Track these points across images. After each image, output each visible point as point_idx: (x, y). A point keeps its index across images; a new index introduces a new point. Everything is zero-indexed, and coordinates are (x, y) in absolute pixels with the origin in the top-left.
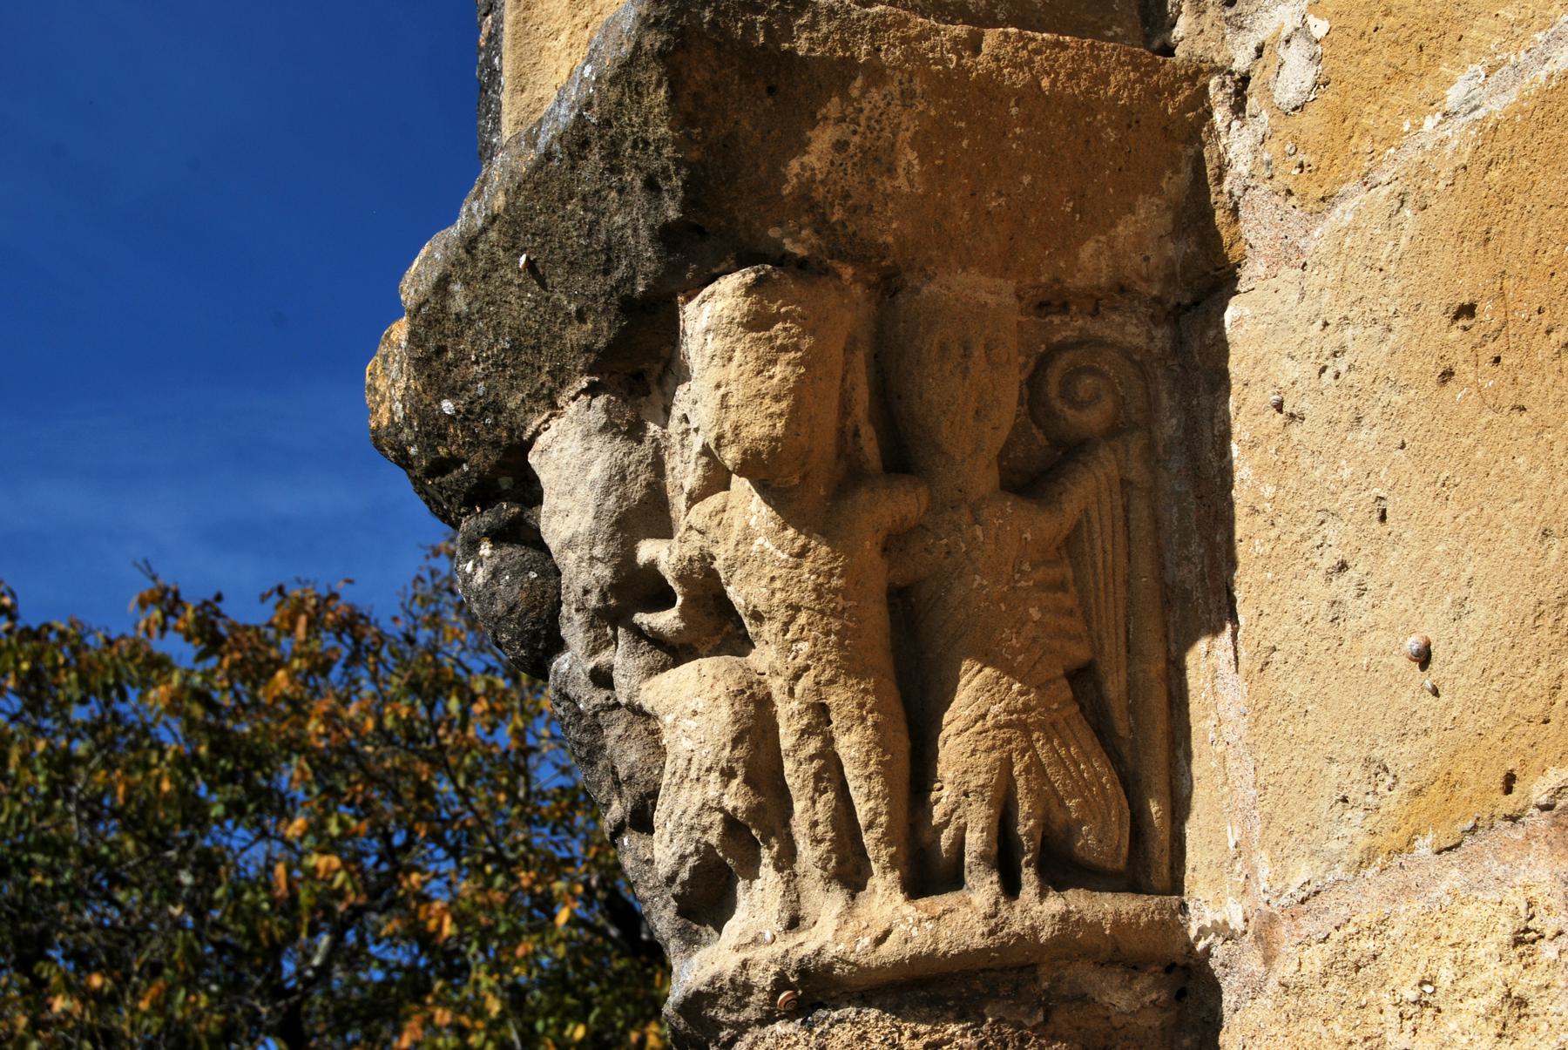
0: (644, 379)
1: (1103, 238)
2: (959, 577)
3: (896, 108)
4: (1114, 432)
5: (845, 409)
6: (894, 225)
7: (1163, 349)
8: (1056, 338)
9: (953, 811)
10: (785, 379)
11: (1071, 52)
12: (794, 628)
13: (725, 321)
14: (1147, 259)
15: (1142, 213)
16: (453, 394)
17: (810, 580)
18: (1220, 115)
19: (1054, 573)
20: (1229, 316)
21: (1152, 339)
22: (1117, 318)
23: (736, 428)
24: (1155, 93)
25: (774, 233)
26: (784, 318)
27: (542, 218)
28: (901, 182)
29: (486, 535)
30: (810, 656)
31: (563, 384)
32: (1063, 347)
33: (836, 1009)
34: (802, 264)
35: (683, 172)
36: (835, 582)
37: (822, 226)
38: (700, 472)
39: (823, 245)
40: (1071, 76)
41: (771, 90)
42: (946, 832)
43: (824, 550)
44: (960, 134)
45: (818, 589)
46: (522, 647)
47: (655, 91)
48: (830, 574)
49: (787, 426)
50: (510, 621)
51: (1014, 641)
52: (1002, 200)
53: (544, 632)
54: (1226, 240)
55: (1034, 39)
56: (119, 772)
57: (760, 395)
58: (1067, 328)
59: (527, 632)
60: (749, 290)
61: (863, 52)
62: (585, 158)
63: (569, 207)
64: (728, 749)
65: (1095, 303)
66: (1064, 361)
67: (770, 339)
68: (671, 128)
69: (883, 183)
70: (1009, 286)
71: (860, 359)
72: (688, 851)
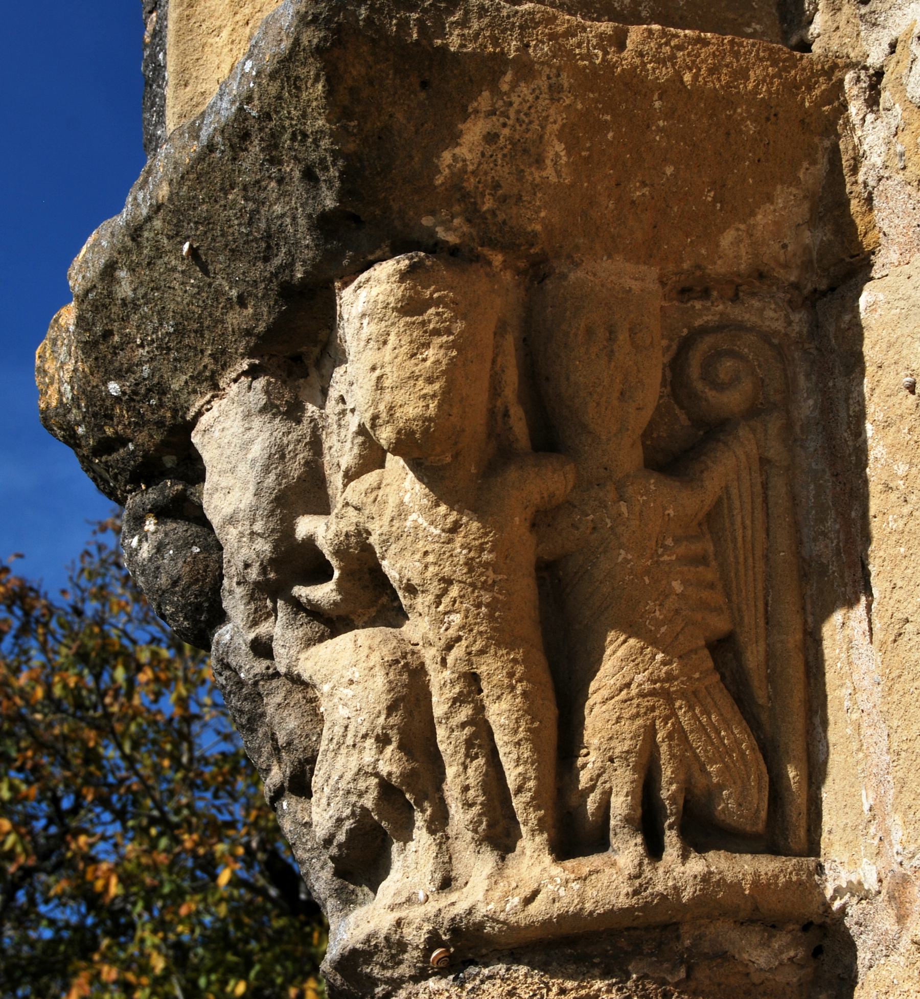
0: (302, 362)
1: (742, 227)
2: (605, 552)
5: (495, 390)
6: (543, 214)
7: (800, 333)
8: (698, 323)
9: (599, 776)
10: (437, 362)
11: (712, 48)
12: (446, 600)
13: (380, 306)
15: (780, 203)
16: (119, 376)
17: (461, 555)
18: (855, 109)
19: (696, 548)
22: (756, 304)
23: (391, 409)
24: (793, 87)
25: (427, 221)
26: (437, 303)
27: (205, 207)
29: (150, 511)
30: (462, 628)
31: (224, 367)
32: (704, 331)
33: (486, 965)
34: (454, 251)
35: (340, 163)
36: (486, 556)
37: (473, 215)
38: (356, 450)
39: (475, 233)
41: (424, 85)
42: (592, 796)
44: (605, 126)
46: (186, 618)
47: (313, 85)
48: (481, 549)
50: (174, 593)
51: (657, 613)
52: (646, 190)
53: (206, 604)
54: (861, 228)
55: (676, 36)
57: (414, 377)
59: (190, 604)
60: (403, 276)
61: (512, 48)
62: (246, 150)
63: (230, 197)
64: (383, 717)
66: (704, 345)
67: (423, 323)
68: (328, 121)
69: (532, 173)
72: (344, 815)
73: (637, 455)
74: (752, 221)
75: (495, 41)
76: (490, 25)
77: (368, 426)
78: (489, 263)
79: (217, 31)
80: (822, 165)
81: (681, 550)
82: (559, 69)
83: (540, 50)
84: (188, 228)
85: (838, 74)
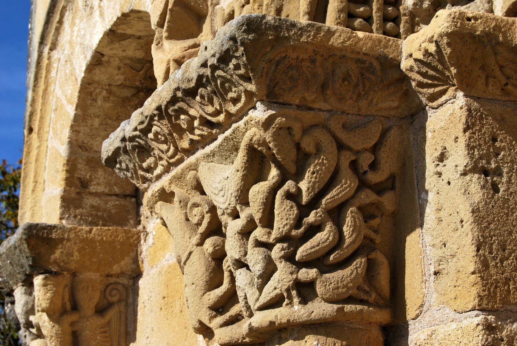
3: (73, 245)
4: (120, 301)
5: (63, 299)
6: (74, 265)
8: (110, 282)
10: (49, 296)
11: (111, 231)
12: (52, 340)
14: (128, 268)
15: (126, 260)
17: (54, 331)
18: (142, 242)
21: (129, 282)
22: (122, 278)
23: (40, 305)
24: (129, 238)
25: (50, 267)
26: (50, 284)
28: (75, 258)
32: (111, 284)
34: (56, 273)
36: (59, 332)
37: (59, 266)
40: (111, 236)
41: (48, 244)
43: (57, 326)
44: (87, 249)
45: (56, 334)
48: (58, 331)
49: (49, 305)
52: (96, 260)
55: (103, 229)
57: (44, 299)
58: (112, 280)
60: (44, 279)
61: (66, 236)
65: (118, 276)
66: (110, 287)
67: (47, 288)
71: (67, 290)
73: (93, 311)
75: (62, 235)
76: (62, 232)
78: (63, 274)
79: (29, 198)
81: (100, 330)
82: (76, 240)
83: (72, 236)
84: (9, 258)
85: (140, 234)
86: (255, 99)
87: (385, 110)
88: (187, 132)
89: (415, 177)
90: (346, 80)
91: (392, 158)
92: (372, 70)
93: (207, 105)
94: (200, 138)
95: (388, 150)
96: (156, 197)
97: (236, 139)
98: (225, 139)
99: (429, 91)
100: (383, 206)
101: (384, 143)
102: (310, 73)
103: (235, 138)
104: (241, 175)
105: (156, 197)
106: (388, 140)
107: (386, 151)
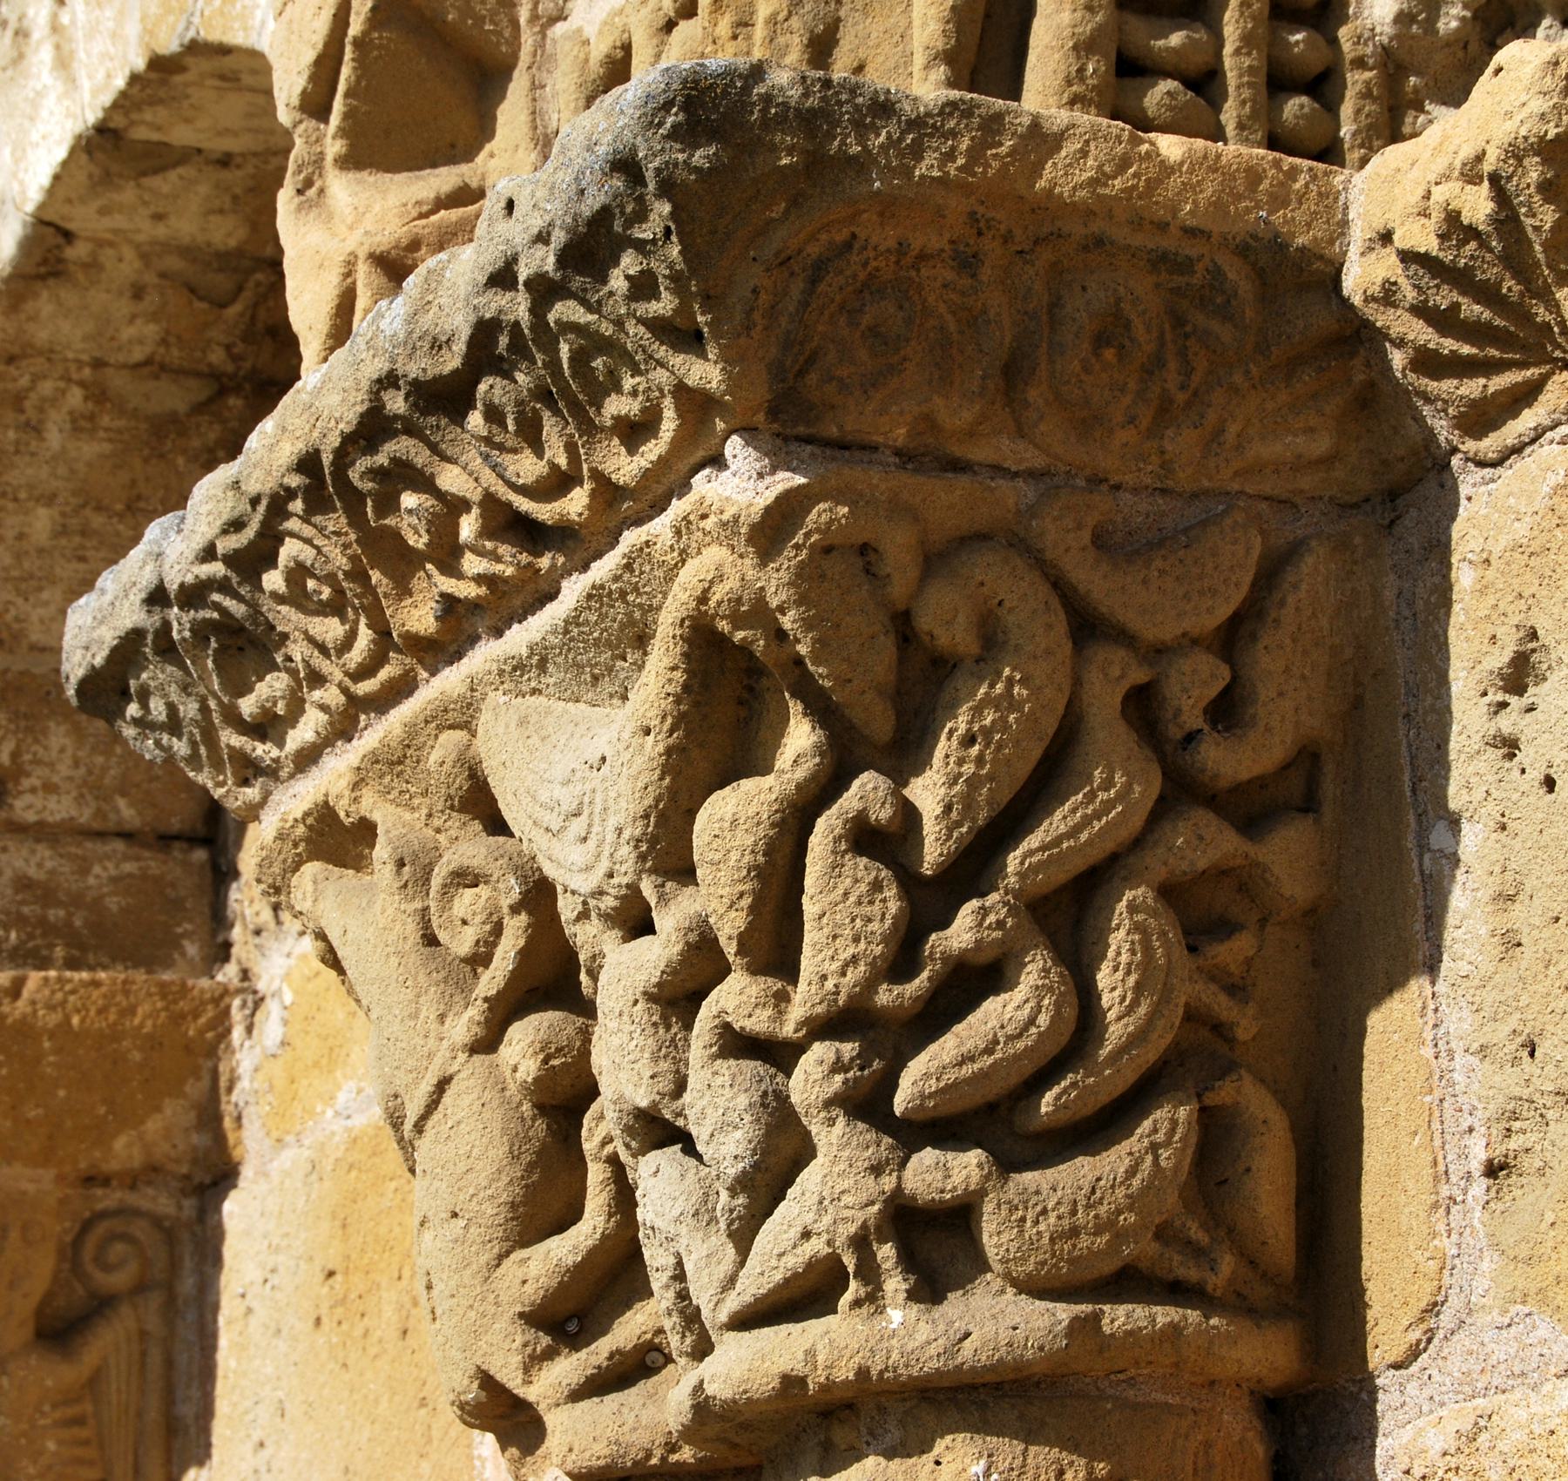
1: (133, 1133)
4: (140, 1288)
8: (100, 1206)
14: (175, 1146)
18: (237, 1034)
19: (71, 1412)
20: (227, 1206)
21: (180, 1208)
22: (150, 1191)
24: (178, 1019)
32: (103, 1215)
40: (101, 1011)
55: (70, 981)
56: (114, 759)
58: (109, 1199)
65: (133, 1180)
66: (101, 1229)
70: (48, 1175)
74: (142, 1128)
77: (327, 459)
80: (205, 1082)
81: (58, 1414)
85: (227, 1000)
86: (720, 425)
87: (1276, 471)
88: (429, 566)
89: (1405, 760)
90: (1108, 344)
91: (1303, 677)
92: (1219, 301)
93: (515, 451)
94: (482, 591)
95: (1288, 641)
96: (296, 845)
97: (639, 594)
98: (589, 597)
99: (1463, 391)
100: (1268, 884)
101: (1273, 614)
102: (954, 313)
103: (636, 589)
104: (661, 748)
105: (296, 845)
106: (1290, 600)
107: (1280, 647)
